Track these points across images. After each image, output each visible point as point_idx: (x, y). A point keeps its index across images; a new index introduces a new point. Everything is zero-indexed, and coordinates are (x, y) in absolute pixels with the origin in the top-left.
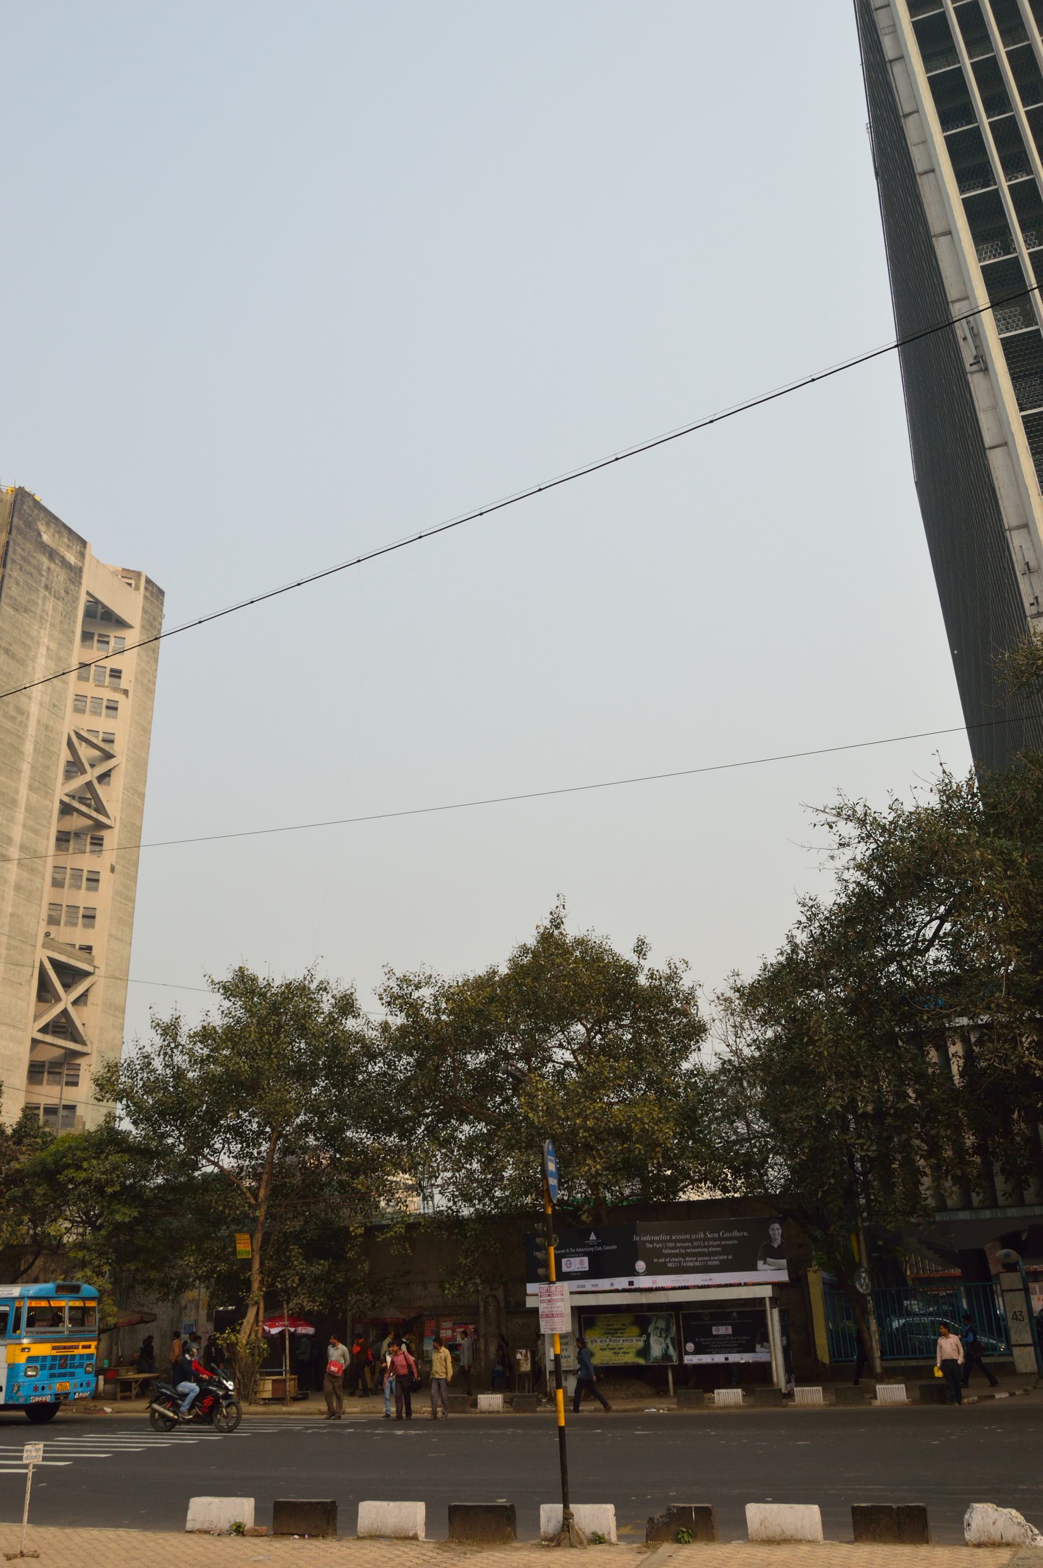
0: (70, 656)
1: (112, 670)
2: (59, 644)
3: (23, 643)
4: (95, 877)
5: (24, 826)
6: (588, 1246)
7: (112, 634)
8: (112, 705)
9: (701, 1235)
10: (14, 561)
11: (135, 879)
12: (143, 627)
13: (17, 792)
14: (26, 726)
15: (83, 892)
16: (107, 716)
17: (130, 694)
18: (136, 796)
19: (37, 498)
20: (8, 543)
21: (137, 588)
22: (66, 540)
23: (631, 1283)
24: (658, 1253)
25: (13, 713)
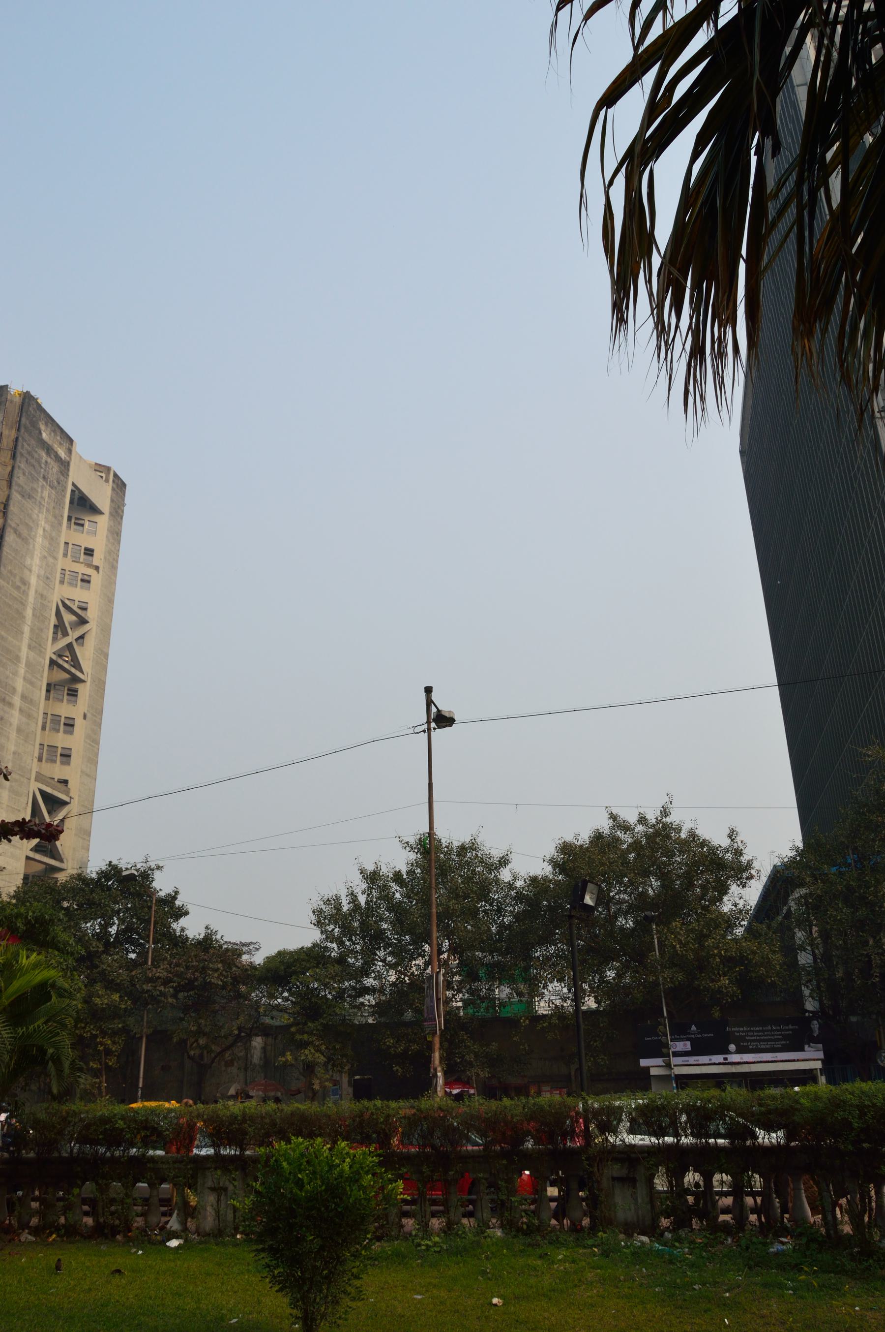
0: (60, 536)
1: (86, 549)
2: (52, 526)
3: (27, 525)
4: (71, 722)
5: (24, 678)
6: (690, 1034)
7: (87, 519)
8: (86, 577)
9: (769, 1028)
10: (22, 455)
11: (99, 725)
12: (111, 514)
13: (20, 650)
14: (28, 595)
15: (61, 734)
16: (82, 587)
17: (101, 570)
18: (103, 655)
19: (39, 401)
20: (17, 438)
21: (107, 481)
22: (59, 438)
23: (725, 1059)
24: (743, 1039)
25: (19, 584)
